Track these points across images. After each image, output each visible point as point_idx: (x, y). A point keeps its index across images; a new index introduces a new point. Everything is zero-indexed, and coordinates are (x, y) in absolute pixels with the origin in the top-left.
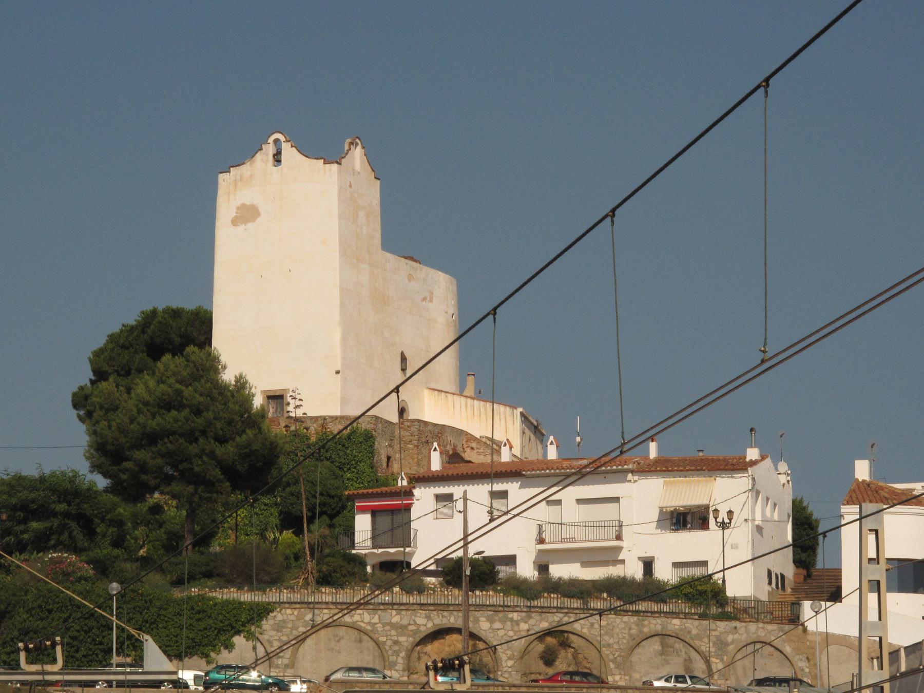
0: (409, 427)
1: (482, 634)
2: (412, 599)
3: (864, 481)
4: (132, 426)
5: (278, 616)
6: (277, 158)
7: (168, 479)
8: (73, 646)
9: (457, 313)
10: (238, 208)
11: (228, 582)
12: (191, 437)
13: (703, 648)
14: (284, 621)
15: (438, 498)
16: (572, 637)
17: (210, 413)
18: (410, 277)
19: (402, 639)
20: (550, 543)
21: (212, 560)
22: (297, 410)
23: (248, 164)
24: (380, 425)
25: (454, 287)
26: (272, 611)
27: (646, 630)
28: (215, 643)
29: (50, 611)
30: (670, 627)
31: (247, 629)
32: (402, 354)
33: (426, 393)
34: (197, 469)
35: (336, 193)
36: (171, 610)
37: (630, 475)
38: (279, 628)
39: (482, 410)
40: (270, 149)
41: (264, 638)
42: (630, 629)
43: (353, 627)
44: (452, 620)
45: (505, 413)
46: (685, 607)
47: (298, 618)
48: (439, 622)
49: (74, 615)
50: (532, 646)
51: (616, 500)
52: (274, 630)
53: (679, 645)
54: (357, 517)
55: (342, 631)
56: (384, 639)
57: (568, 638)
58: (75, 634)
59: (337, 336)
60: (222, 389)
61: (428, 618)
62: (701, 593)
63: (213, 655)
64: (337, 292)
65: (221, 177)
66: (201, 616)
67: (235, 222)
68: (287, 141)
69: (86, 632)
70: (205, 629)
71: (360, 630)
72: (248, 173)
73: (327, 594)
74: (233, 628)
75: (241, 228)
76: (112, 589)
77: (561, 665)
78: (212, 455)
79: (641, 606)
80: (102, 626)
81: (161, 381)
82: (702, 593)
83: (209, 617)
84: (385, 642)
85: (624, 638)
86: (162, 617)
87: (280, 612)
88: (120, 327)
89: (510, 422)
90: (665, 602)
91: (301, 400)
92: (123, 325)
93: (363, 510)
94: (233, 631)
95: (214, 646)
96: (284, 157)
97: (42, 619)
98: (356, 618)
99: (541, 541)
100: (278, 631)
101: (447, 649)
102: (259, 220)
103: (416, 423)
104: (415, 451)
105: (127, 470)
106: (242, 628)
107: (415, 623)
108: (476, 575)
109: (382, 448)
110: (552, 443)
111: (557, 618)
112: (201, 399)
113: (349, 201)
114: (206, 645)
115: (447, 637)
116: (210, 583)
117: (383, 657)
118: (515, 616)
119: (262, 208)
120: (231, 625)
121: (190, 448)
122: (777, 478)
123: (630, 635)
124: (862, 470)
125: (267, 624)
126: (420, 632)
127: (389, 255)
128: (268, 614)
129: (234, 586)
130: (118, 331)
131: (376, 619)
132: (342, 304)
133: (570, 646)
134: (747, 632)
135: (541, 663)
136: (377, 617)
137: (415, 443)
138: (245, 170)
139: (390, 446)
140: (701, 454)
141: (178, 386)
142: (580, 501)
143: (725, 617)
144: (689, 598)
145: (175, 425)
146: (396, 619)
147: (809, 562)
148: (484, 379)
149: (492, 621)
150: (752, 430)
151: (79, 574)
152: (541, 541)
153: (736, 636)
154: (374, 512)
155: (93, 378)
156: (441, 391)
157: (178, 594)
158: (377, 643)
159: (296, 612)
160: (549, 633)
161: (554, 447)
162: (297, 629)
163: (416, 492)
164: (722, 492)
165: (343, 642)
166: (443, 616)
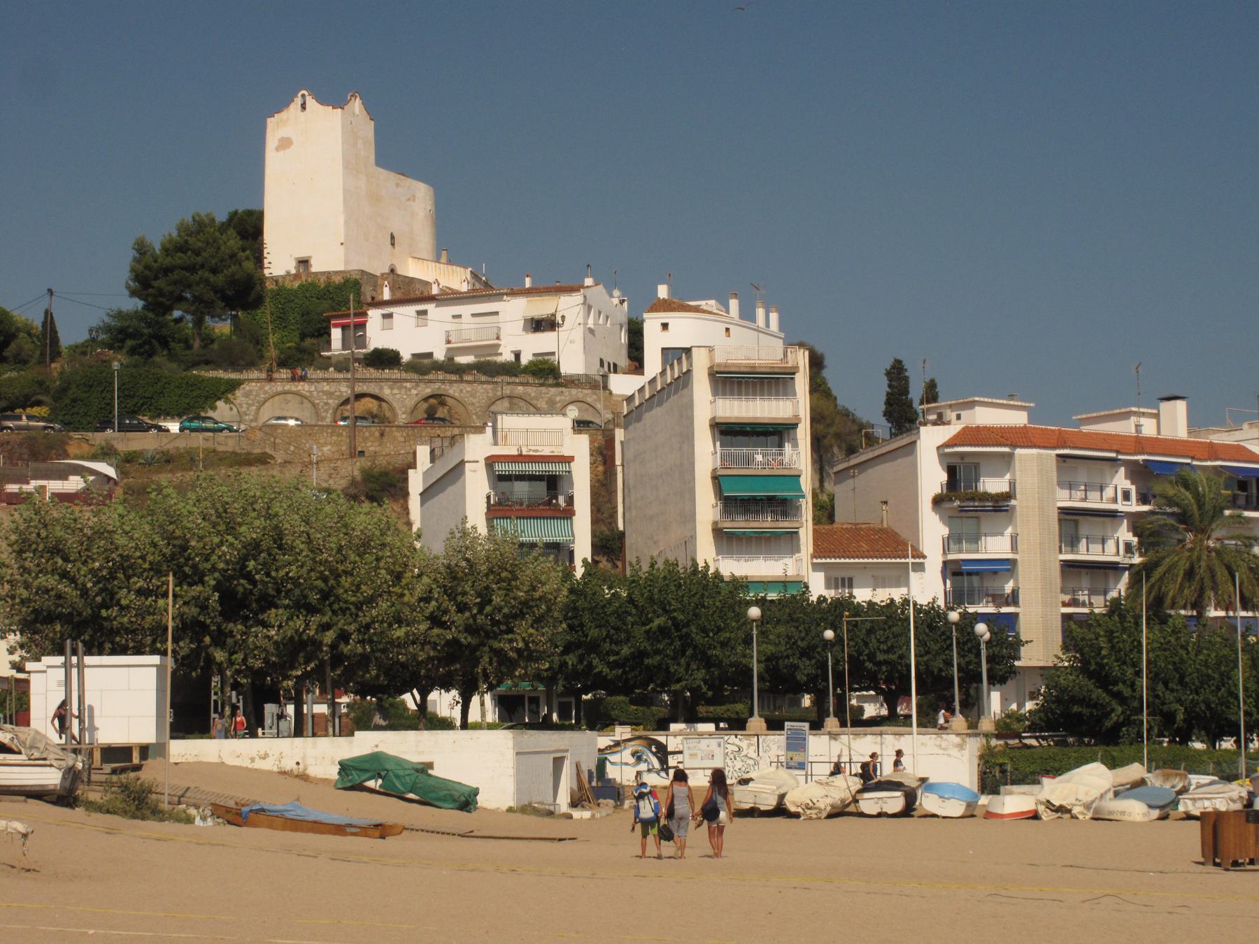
1: (385, 398)
5: (246, 387)
6: (303, 107)
7: (181, 299)
12: (192, 269)
18: (397, 185)
29: (91, 386)
33: (410, 260)
38: (247, 395)
40: (299, 100)
43: (297, 394)
46: (531, 380)
47: (261, 388)
51: (497, 313)
55: (289, 397)
59: (341, 220)
62: (545, 370)
64: (341, 192)
65: (269, 120)
67: (277, 149)
75: (281, 153)
78: (207, 282)
79: (499, 379)
82: (541, 370)
90: (516, 376)
93: (336, 326)
96: (881, 388)
98: (300, 388)
108: (384, 359)
111: (437, 385)
113: (350, 135)
117: (317, 414)
118: (408, 385)
122: (615, 306)
124: (663, 292)
125: (238, 393)
131: (313, 388)
138: (283, 115)
142: (473, 315)
143: (558, 385)
144: (534, 374)
146: (327, 388)
148: (448, 246)
149: (392, 388)
152: (449, 342)
154: (344, 328)
158: (314, 405)
160: (432, 396)
164: (568, 306)
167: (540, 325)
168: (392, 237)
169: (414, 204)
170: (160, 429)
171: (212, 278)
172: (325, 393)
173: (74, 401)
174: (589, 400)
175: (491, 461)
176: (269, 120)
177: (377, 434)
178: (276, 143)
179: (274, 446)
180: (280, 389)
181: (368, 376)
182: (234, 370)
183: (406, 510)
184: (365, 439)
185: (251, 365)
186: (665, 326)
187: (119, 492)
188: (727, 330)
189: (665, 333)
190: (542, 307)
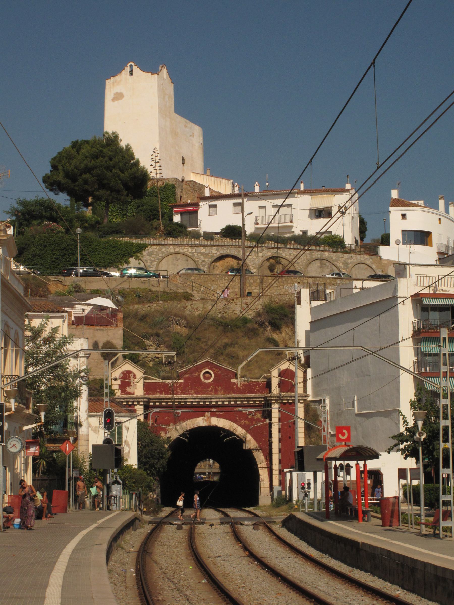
3: (396, 199)
5: (150, 249)
6: (131, 73)
8: (56, 263)
10: (114, 94)
12: (108, 168)
13: (338, 265)
14: (152, 251)
15: (211, 207)
16: (282, 260)
17: (116, 159)
18: (185, 126)
19: (206, 260)
20: (261, 224)
22: (156, 158)
26: (147, 247)
27: (314, 257)
29: (45, 246)
30: (324, 256)
32: (183, 157)
36: (101, 246)
37: (296, 194)
38: (150, 254)
39: (216, 181)
40: (128, 69)
41: (144, 259)
42: (307, 256)
44: (228, 251)
46: (328, 248)
49: (56, 248)
50: (264, 263)
52: (148, 255)
53: (328, 264)
55: (179, 256)
56: (198, 260)
57: (280, 260)
61: (218, 250)
63: (120, 267)
64: (157, 128)
65: (107, 81)
66: (114, 249)
67: (113, 100)
68: (135, 65)
69: (62, 256)
70: (117, 255)
73: (170, 241)
74: (129, 254)
75: (116, 102)
76: (78, 231)
77: (279, 269)
78: (119, 176)
81: (92, 147)
82: (335, 242)
83: (119, 249)
85: (304, 260)
88: (63, 148)
89: (227, 187)
90: (319, 246)
92: (64, 148)
93: (177, 212)
94: (129, 256)
95: (121, 262)
96: (134, 73)
97: (41, 250)
98: (185, 250)
99: (257, 224)
101: (226, 264)
102: (124, 99)
107: (212, 253)
110: (257, 185)
113: (161, 90)
114: (117, 262)
115: (226, 259)
116: (118, 236)
119: (125, 93)
120: (128, 253)
123: (307, 259)
124: (395, 194)
125: (145, 253)
126: (214, 256)
127: (177, 115)
128: (145, 248)
129: (128, 237)
131: (194, 251)
132: (159, 133)
133: (281, 264)
134: (357, 259)
135: (268, 271)
136: (194, 250)
138: (118, 78)
139: (182, 192)
140: (324, 188)
141: (101, 149)
143: (346, 252)
144: (329, 245)
145: (102, 163)
146: (203, 251)
147: (372, 238)
148: (212, 167)
150: (347, 176)
153: (352, 260)
155: (52, 170)
160: (271, 258)
161: (258, 187)
162: (158, 255)
163: (201, 204)
164: (335, 201)
165: (179, 261)
166: (224, 250)
167: (320, 213)
168: (183, 159)
169: (193, 138)
170: (108, 275)
171: (121, 175)
172: (202, 254)
173: (34, 256)
174: (368, 263)
175: (417, 299)
176: (107, 81)
177: (258, 281)
179: (192, 288)
180: (172, 250)
182: (137, 238)
183: (294, 332)
184: (251, 284)
186: (404, 216)
187: (120, 316)
188: (440, 219)
189: (404, 220)
190: (321, 201)
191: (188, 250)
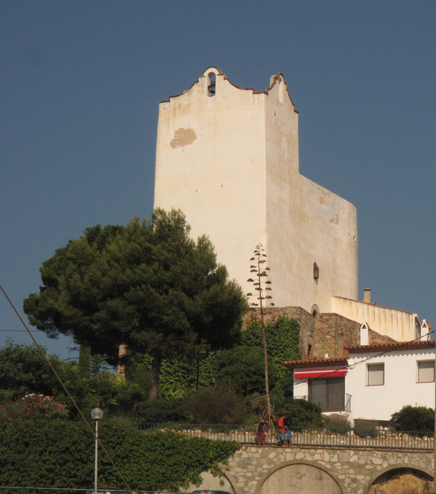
0: (327, 320)
2: (364, 443)
4: (104, 279)
5: (243, 454)
6: (212, 90)
9: (357, 236)
11: (194, 424)
12: (158, 285)
14: (249, 459)
15: (371, 367)
18: (322, 200)
19: (359, 477)
21: (178, 404)
22: (261, 265)
23: (186, 94)
24: (304, 316)
25: (355, 213)
26: (238, 449)
28: (183, 477)
29: (27, 445)
31: (214, 466)
32: (315, 265)
33: (333, 300)
34: (165, 318)
35: (264, 119)
36: (142, 445)
38: (244, 465)
39: (382, 315)
40: (205, 81)
44: (406, 460)
45: (402, 318)
47: (263, 456)
48: (395, 463)
52: (239, 466)
54: (294, 386)
55: (303, 469)
56: (343, 477)
58: (52, 466)
60: (188, 247)
61: (384, 458)
64: (264, 204)
65: (162, 106)
66: (171, 452)
67: (174, 144)
68: (220, 75)
69: (61, 465)
70: (175, 464)
71: (320, 468)
72: (186, 102)
74: (201, 464)
75: (179, 149)
76: (95, 415)
78: (181, 305)
80: (76, 459)
83: (179, 453)
84: (343, 480)
86: (134, 453)
87: (245, 450)
88: (67, 242)
91: (264, 255)
93: (301, 379)
94: (201, 467)
95: (183, 481)
97: (19, 453)
98: (317, 457)
100: (243, 468)
102: (195, 142)
103: (334, 317)
104: (333, 341)
105: (99, 320)
106: (209, 465)
107: (372, 463)
109: (305, 335)
112: (169, 255)
114: (176, 480)
115: (401, 477)
119: (197, 131)
120: (199, 461)
121: (161, 298)
125: (233, 461)
126: (377, 471)
127: (305, 178)
128: (234, 452)
130: (65, 246)
131: (335, 459)
132: (268, 215)
136: (336, 456)
137: (333, 334)
138: (183, 99)
141: (147, 244)
145: (145, 276)
146: (354, 459)
148: (374, 286)
151: (55, 412)
155: (43, 286)
156: (347, 299)
157: (145, 433)
158: (336, 481)
159: (260, 451)
162: (261, 467)
165: (304, 479)
166: (398, 457)
168: (316, 269)
171: (188, 302)
172: (352, 465)
176: (162, 106)
178: (172, 136)
181: (400, 444)
182: (217, 430)
185: (238, 424)
191: (323, 457)
